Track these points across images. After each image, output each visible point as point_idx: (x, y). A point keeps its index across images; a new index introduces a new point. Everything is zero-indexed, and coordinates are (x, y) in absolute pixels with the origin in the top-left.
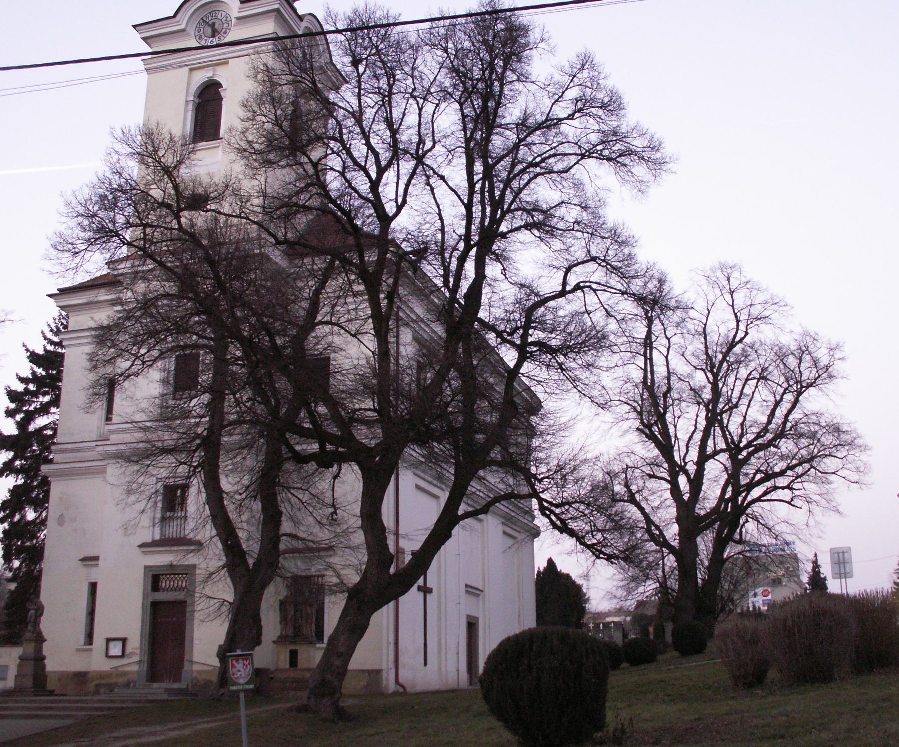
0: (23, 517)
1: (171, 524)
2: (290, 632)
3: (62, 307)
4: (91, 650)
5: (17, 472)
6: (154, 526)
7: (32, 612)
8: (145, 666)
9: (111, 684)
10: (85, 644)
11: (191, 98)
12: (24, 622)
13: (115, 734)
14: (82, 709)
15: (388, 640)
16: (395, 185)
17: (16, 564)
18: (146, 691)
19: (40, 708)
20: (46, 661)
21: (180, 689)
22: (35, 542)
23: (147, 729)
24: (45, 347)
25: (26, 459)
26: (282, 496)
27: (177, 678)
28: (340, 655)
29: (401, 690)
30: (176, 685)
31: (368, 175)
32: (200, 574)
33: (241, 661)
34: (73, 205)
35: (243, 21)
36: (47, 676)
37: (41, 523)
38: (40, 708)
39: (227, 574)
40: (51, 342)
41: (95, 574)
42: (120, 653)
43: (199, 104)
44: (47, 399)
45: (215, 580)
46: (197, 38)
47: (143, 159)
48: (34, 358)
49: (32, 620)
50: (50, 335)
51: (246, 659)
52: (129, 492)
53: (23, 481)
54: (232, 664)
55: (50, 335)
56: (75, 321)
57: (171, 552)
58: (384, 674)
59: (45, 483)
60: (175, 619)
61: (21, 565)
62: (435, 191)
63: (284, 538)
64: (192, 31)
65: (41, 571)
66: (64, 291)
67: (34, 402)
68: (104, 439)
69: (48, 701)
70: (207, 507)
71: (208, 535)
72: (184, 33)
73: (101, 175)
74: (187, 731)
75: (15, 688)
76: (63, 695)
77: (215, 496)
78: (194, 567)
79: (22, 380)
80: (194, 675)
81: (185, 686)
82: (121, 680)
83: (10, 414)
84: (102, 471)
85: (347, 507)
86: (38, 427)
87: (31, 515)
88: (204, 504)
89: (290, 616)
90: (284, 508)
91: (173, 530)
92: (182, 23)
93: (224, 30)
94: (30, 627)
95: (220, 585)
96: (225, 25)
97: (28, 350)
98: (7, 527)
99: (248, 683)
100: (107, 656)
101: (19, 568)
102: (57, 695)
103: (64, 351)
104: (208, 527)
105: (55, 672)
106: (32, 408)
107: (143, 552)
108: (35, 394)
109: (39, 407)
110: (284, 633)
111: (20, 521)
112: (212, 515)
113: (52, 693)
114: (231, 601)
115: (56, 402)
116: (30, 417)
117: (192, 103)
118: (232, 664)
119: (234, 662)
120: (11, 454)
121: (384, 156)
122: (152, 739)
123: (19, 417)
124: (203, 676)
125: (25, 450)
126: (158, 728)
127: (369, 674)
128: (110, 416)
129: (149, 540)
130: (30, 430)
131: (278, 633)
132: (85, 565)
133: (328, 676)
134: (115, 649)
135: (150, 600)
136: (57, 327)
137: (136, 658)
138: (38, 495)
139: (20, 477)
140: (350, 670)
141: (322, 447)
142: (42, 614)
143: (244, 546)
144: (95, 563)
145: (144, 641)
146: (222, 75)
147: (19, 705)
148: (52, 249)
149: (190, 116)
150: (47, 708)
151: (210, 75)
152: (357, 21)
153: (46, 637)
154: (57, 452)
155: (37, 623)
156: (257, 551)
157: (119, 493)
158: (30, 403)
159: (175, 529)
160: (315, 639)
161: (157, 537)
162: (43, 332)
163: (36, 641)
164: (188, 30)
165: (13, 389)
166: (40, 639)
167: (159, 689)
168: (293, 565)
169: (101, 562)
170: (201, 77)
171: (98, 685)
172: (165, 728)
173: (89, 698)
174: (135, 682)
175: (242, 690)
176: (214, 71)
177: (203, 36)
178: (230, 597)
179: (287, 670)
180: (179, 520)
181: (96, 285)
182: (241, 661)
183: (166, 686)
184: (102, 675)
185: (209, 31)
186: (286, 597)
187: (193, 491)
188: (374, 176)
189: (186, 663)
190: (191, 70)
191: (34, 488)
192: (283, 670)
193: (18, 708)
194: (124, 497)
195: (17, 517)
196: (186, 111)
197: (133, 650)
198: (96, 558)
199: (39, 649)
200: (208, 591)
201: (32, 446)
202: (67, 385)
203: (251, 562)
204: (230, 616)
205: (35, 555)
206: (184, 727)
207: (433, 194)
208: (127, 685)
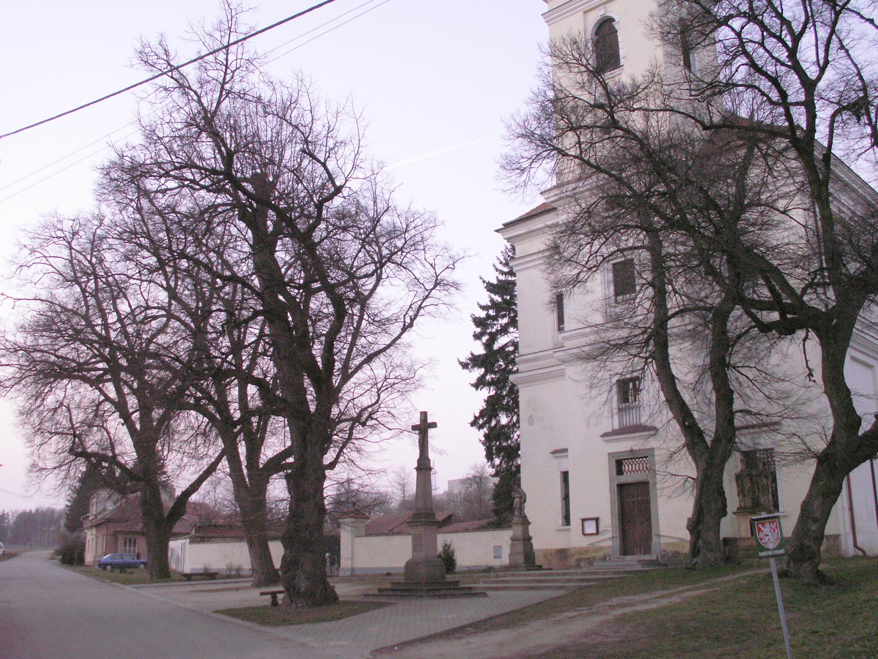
0: (498, 422)
1: (631, 412)
2: (749, 503)
3: (508, 240)
4: (569, 530)
5: (489, 384)
6: (612, 417)
7: (517, 500)
9: (589, 559)
10: (563, 525)
12: (511, 508)
13: (608, 603)
14: (570, 581)
15: (842, 505)
16: (814, 48)
17: (497, 461)
18: (621, 563)
19: (533, 581)
20: (532, 541)
21: (652, 561)
22: (509, 442)
23: (636, 598)
24: (497, 278)
25: (495, 373)
26: (731, 374)
27: (648, 551)
28: (815, 520)
29: (860, 553)
30: (647, 557)
31: (785, 44)
32: (660, 456)
33: (767, 525)
34: (513, 128)
36: (534, 554)
37: (514, 426)
38: (533, 581)
39: (687, 453)
40: (502, 273)
41: (564, 464)
42: (595, 531)
44: (505, 320)
45: (677, 459)
48: (491, 288)
49: (518, 507)
50: (500, 267)
51: (773, 522)
52: (591, 387)
53: (494, 392)
54: (758, 527)
55: (500, 267)
56: (522, 249)
57: (629, 439)
58: (843, 539)
59: (514, 392)
60: (639, 498)
61: (501, 462)
62: (850, 52)
63: (738, 414)
65: (518, 467)
66: (507, 225)
67: (495, 324)
68: (559, 347)
69: (540, 575)
70: (661, 393)
71: (665, 419)
73: (535, 90)
74: (676, 599)
75: (510, 564)
76: (550, 569)
77: (668, 380)
78: (652, 449)
79: (483, 308)
80: (663, 547)
81: (654, 558)
83: (477, 337)
84: (561, 375)
85: (797, 379)
86: (501, 346)
87: (504, 420)
88: (658, 391)
89: (747, 488)
90: (734, 386)
91: (630, 419)
94: (516, 513)
95: (682, 463)
97: (484, 282)
98: (487, 432)
99: (778, 548)
100: (584, 534)
101: (500, 465)
102: (544, 569)
103: (513, 278)
104: (664, 412)
105: (541, 550)
106: (494, 330)
108: (495, 318)
109: (499, 328)
110: (742, 504)
111: (495, 426)
112: (667, 400)
113: (540, 567)
114: (695, 477)
115: (513, 322)
116: (493, 338)
118: (758, 527)
119: (760, 526)
120: (483, 370)
121: (588, 266)
122: (646, 607)
123: (485, 338)
124: (671, 548)
125: (493, 365)
126: (647, 597)
128: (561, 326)
129: (610, 430)
130: (495, 349)
131: (738, 505)
132: (556, 457)
133: (807, 542)
134: (590, 528)
135: (616, 483)
137: (610, 535)
138: (508, 402)
139: (492, 388)
140: (827, 537)
141: (783, 315)
142: (525, 501)
143: (700, 425)
144: (565, 454)
147: (516, 578)
148: (501, 170)
150: (541, 581)
151: (602, 12)
152: (299, 605)
153: (530, 520)
154: (525, 361)
155: (521, 509)
156: (713, 430)
157: (582, 389)
158: (492, 325)
159: (634, 417)
160: (772, 508)
161: (616, 427)
162: (494, 265)
163: (523, 524)
165: (477, 316)
166: (525, 522)
167: (633, 561)
168: (745, 441)
169: (570, 453)
170: (594, 18)
171: (578, 560)
172: (653, 596)
173: (572, 571)
174: (610, 556)
175: (773, 556)
178: (694, 474)
179: (749, 539)
180: (637, 409)
181: (534, 215)
182: (767, 525)
183: (638, 559)
184: (581, 551)
186: (742, 471)
187: (648, 377)
188: (790, 44)
189: (654, 537)
190: (585, 12)
191: (503, 397)
192: (745, 539)
193: (513, 582)
194: (587, 390)
195: (493, 423)
198: (566, 450)
199: (526, 531)
200: (671, 469)
201: (498, 361)
202: (522, 305)
203: (708, 440)
204: (695, 491)
205: (512, 452)
206: (672, 595)
207: (849, 55)
208: (604, 558)
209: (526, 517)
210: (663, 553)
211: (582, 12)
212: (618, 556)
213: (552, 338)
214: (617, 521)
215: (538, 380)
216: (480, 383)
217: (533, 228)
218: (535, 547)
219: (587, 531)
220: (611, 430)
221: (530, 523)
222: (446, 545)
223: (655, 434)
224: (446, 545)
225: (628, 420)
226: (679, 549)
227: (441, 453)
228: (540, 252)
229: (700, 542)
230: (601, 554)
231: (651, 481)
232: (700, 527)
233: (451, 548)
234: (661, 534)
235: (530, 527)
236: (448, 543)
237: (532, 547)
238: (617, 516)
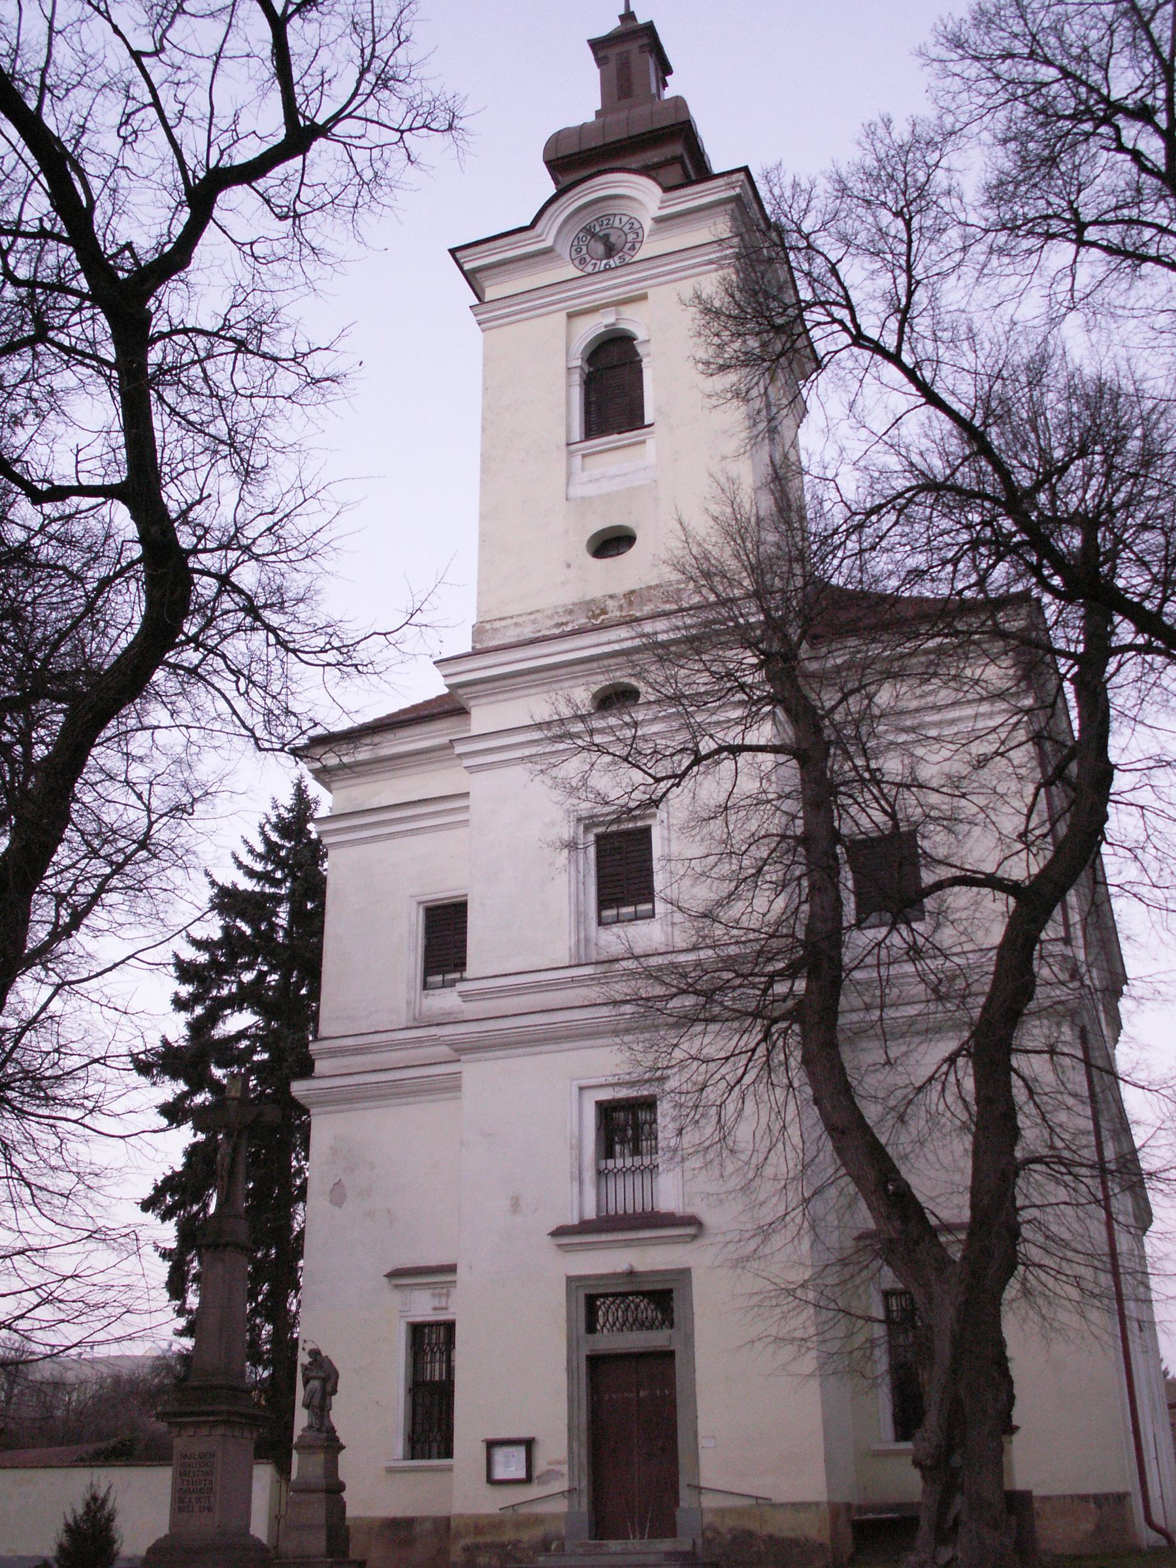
4: (450, 1469)
8: (584, 1504)
9: (503, 1546)
10: (405, 1458)
11: (578, 363)
20: (345, 1495)
27: (665, 1526)
35: (667, 224)
42: (522, 1474)
43: (589, 375)
46: (577, 262)
47: (944, 69)
50: (248, 860)
57: (628, 1243)
64: (564, 250)
72: (552, 255)
80: (708, 1519)
81: (687, 1547)
82: (528, 1536)
92: (548, 235)
93: (628, 245)
96: (631, 237)
97: (213, 883)
100: (491, 1481)
107: (559, 1246)
116: (214, 1016)
117: (578, 371)
124: (730, 1522)
127: (1099, 1506)
132: (397, 1286)
134: (510, 1465)
135: (585, 1351)
136: (267, 840)
137: (563, 1485)
142: (334, 1392)
144: (449, 1278)
145: (575, 1444)
146: (635, 321)
149: (577, 394)
161: (590, 1213)
164: (558, 249)
169: (462, 1274)
170: (591, 328)
174: (559, 1537)
176: (618, 313)
177: (588, 259)
180: (647, 1175)
184: (479, 1525)
185: (600, 249)
189: (684, 1492)
190: (570, 316)
196: (569, 386)
197: (551, 1467)
199: (332, 1467)
209: (332, 1430)
210: (709, 1534)
211: (563, 314)
212: (585, 1534)
213: (409, 1003)
214: (584, 1451)
215: (366, 1099)
216: (173, 1113)
217: (385, 751)
218: (350, 1512)
219: (500, 1473)
220: (576, 1221)
221: (342, 1447)
222: (94, 1498)
223: (694, 1237)
224: (94, 1498)
225: (638, 1195)
226: (752, 1526)
227: (1128, 938)
228: (539, 726)
229: (959, 1503)
230: (538, 1532)
231: (676, 1347)
232: (956, 1460)
233: (109, 1505)
234: (703, 1484)
235: (342, 1456)
236: (101, 1494)
237: (344, 1512)
238: (584, 1437)
